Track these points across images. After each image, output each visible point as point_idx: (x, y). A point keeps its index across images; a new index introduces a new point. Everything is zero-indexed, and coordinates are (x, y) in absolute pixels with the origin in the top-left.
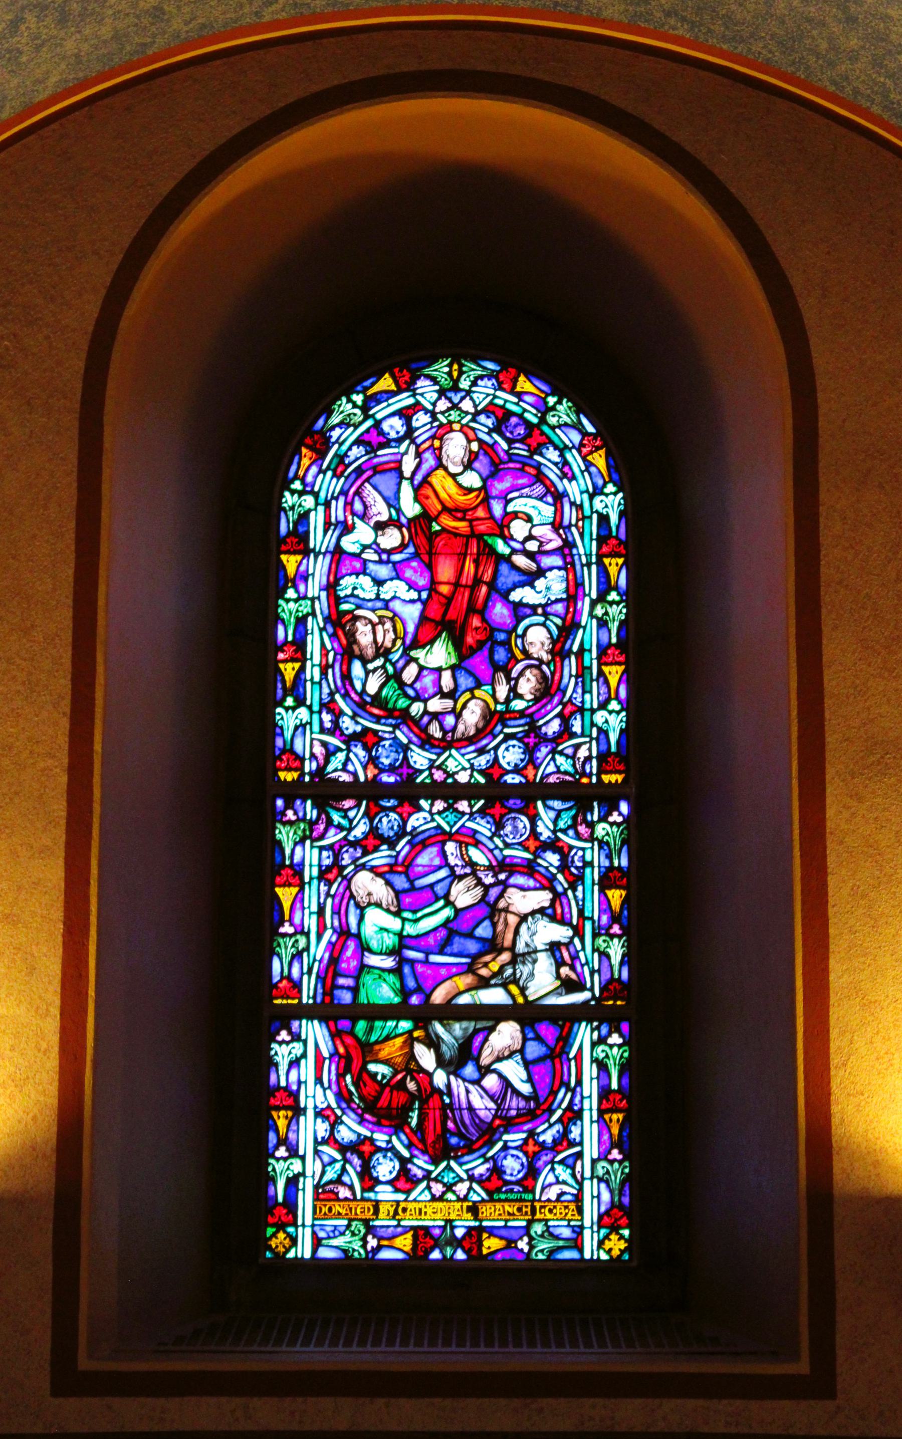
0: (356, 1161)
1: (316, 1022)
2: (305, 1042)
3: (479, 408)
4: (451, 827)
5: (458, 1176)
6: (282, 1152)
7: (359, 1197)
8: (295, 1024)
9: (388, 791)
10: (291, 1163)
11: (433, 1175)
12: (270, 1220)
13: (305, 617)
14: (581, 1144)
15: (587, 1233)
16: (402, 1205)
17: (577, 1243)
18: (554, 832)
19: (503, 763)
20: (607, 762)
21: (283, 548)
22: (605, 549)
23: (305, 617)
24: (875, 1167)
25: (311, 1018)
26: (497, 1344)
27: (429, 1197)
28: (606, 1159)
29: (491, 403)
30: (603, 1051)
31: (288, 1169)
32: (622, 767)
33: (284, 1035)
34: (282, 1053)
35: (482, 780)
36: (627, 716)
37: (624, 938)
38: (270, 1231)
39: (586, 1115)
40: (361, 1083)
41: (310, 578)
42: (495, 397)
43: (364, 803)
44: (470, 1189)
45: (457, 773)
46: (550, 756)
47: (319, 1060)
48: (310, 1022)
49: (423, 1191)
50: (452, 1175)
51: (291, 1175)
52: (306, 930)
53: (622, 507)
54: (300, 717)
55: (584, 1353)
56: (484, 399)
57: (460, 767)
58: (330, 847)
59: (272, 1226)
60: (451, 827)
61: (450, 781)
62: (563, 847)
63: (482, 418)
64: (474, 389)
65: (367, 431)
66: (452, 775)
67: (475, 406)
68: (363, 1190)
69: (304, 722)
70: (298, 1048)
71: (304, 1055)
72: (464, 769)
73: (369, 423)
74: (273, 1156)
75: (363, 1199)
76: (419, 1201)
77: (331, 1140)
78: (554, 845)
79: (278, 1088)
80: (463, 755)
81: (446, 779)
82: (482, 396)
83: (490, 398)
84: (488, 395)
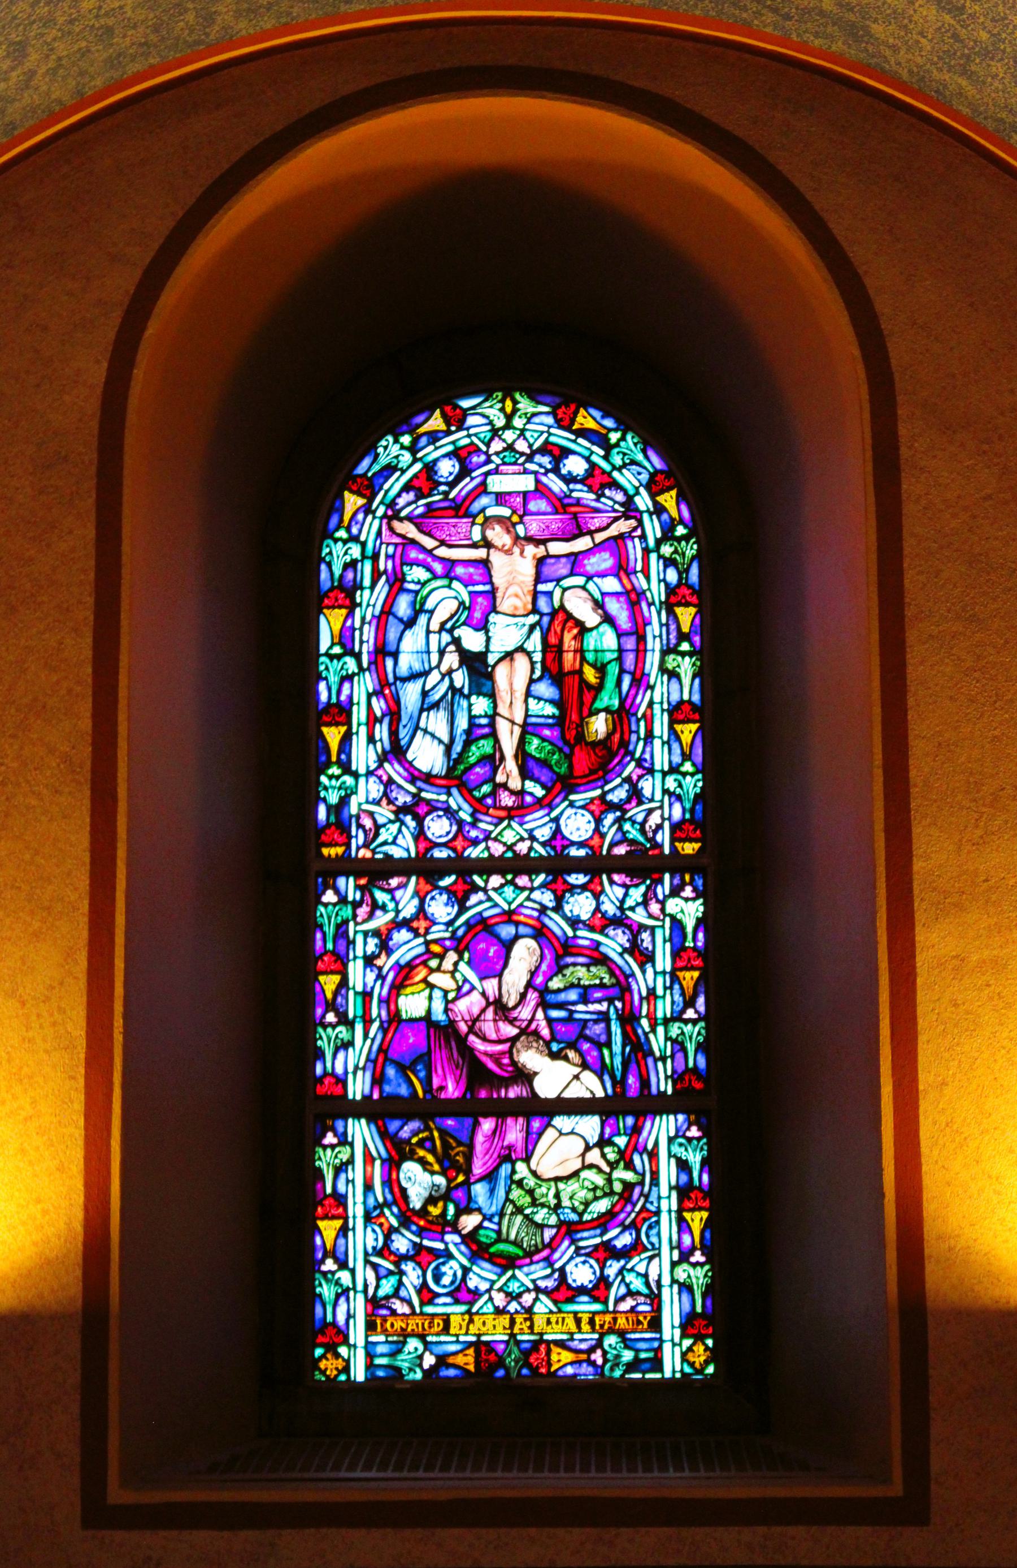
0: (412, 824)
1: (363, 1121)
2: (351, 1145)
3: (535, 447)
4: (510, 904)
5: (523, 1285)
6: (331, 1017)
7: (418, 1310)
8: (340, 1125)
9: (441, 869)
10: (339, 1152)
11: (493, 835)
12: (320, 1339)
13: (345, 922)
14: (659, 1249)
15: (667, 1348)
16: (463, 1331)
17: (657, 1363)
18: (621, 908)
19: (566, 832)
20: (689, 1198)
21: (325, 718)
22: (680, 964)
23: (345, 922)
24: (955, 905)
25: (358, 1116)
26: (593, 1468)
27: (491, 1309)
28: (684, 1136)
29: (547, 442)
30: (684, 1271)
31: (342, 668)
32: (697, 716)
33: (330, 1138)
34: (325, 1160)
35: (476, 878)
36: (706, 1028)
37: (693, 540)
38: (319, 1352)
39: (664, 1217)
40: (418, 607)
41: (350, 1234)
42: (550, 434)
43: (604, 852)
44: (536, 1299)
45: (515, 844)
46: (616, 826)
47: (369, 1159)
48: (356, 1121)
49: (486, 1303)
50: (517, 1284)
51: (348, 560)
52: (350, 1139)
53: (701, 1039)
54: (340, 1036)
55: (581, 1478)
56: (539, 437)
57: (518, 837)
58: (376, 933)
59: (321, 1345)
60: (510, 904)
61: (509, 877)
62: (388, 804)
63: (538, 458)
64: (528, 426)
65: (416, 476)
66: (507, 883)
67: (530, 446)
68: (422, 1304)
69: (350, 672)
70: (344, 1154)
71: (351, 1161)
72: (528, 1290)
73: (418, 466)
74: (331, 536)
75: (422, 1314)
76: (483, 1314)
77: (384, 1251)
78: (620, 921)
79: (325, 1324)
80: (527, 1275)
81: (504, 852)
82: (536, 435)
83: (545, 435)
84: (542, 433)
